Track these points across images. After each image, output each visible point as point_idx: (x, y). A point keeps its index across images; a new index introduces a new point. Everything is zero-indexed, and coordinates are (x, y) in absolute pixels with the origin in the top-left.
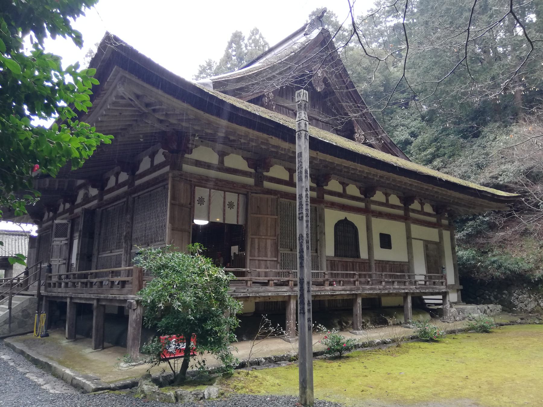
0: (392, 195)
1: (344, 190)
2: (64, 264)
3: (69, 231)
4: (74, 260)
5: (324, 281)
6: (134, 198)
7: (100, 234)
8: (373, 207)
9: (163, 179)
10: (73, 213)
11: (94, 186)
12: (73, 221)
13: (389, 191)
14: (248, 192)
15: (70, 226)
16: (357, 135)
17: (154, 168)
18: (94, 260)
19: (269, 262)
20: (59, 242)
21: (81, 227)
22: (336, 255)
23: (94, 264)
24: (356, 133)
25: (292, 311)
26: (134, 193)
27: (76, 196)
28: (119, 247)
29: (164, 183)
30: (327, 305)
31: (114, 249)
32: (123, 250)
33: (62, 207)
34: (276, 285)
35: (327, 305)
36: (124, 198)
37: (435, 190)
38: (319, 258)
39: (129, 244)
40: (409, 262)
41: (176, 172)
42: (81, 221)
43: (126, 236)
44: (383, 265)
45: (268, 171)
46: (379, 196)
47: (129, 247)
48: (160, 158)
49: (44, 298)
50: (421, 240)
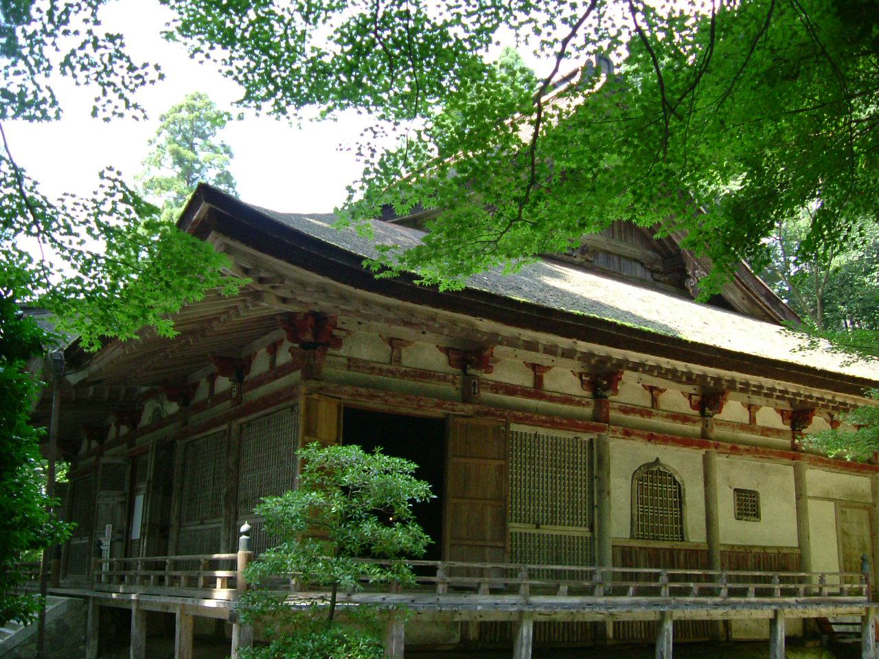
0: (764, 408)
1: (654, 401)
2: (119, 540)
3: (127, 477)
4: (136, 534)
5: (593, 587)
6: (241, 425)
7: (181, 489)
8: (717, 431)
9: (288, 394)
10: (134, 445)
11: (172, 398)
12: (135, 460)
13: (756, 400)
14: (448, 414)
15: (129, 469)
16: (690, 283)
17: (277, 372)
18: (173, 535)
19: (488, 549)
20: (107, 501)
21: (150, 474)
22: (632, 537)
23: (171, 546)
24: (689, 277)
25: (525, 642)
26: (241, 416)
27: (140, 413)
28: (216, 515)
29: (291, 403)
30: (610, 632)
31: (206, 518)
32: (222, 519)
33: (112, 433)
34: (494, 591)
35: (610, 632)
36: (223, 423)
37: (838, 399)
38: (596, 542)
39: (233, 510)
40: (799, 547)
41: (313, 384)
42: (151, 459)
43: (227, 495)
44: (740, 558)
45: (489, 370)
46: (733, 409)
47: (233, 516)
48: (284, 357)
49: (91, 602)
50: (830, 500)
